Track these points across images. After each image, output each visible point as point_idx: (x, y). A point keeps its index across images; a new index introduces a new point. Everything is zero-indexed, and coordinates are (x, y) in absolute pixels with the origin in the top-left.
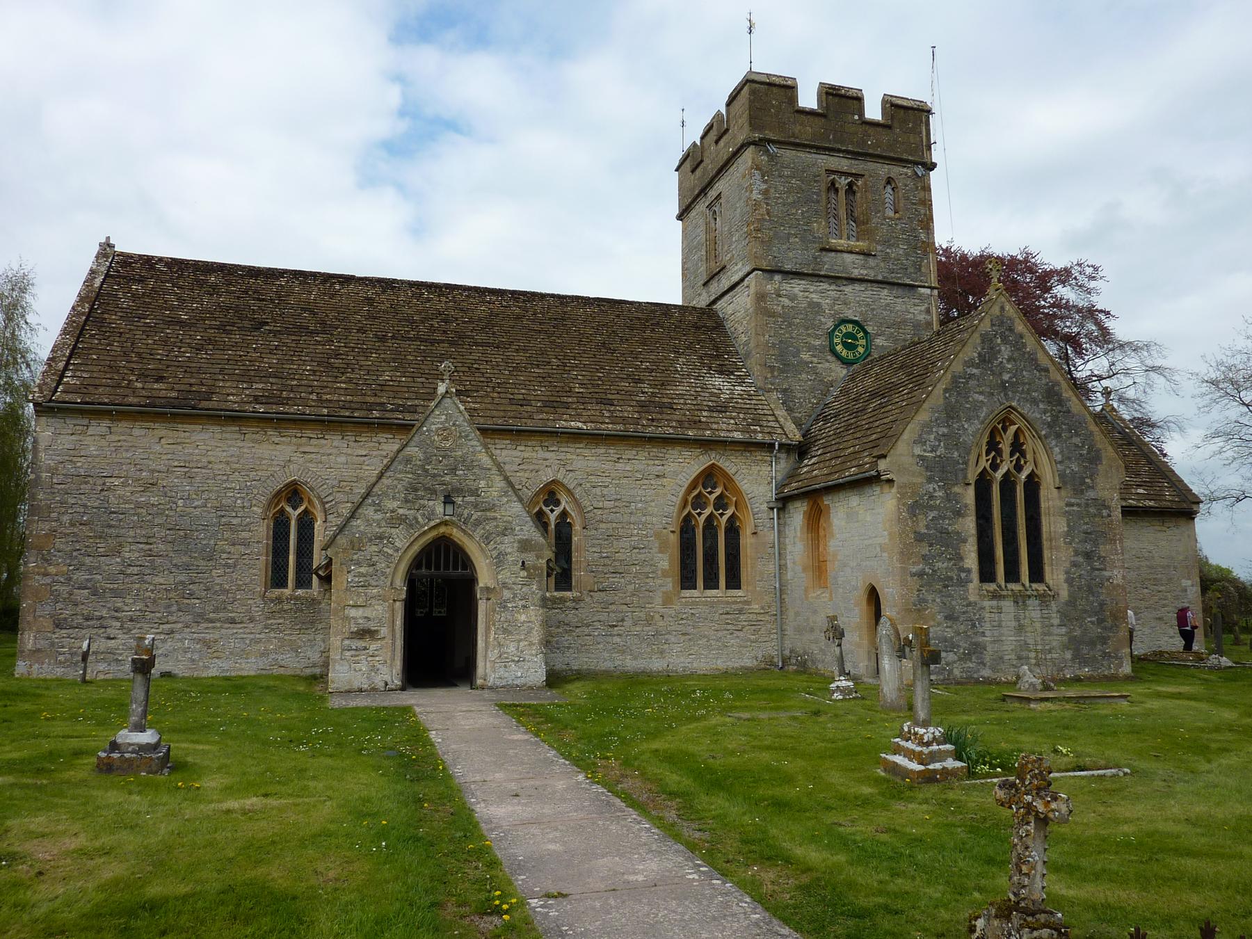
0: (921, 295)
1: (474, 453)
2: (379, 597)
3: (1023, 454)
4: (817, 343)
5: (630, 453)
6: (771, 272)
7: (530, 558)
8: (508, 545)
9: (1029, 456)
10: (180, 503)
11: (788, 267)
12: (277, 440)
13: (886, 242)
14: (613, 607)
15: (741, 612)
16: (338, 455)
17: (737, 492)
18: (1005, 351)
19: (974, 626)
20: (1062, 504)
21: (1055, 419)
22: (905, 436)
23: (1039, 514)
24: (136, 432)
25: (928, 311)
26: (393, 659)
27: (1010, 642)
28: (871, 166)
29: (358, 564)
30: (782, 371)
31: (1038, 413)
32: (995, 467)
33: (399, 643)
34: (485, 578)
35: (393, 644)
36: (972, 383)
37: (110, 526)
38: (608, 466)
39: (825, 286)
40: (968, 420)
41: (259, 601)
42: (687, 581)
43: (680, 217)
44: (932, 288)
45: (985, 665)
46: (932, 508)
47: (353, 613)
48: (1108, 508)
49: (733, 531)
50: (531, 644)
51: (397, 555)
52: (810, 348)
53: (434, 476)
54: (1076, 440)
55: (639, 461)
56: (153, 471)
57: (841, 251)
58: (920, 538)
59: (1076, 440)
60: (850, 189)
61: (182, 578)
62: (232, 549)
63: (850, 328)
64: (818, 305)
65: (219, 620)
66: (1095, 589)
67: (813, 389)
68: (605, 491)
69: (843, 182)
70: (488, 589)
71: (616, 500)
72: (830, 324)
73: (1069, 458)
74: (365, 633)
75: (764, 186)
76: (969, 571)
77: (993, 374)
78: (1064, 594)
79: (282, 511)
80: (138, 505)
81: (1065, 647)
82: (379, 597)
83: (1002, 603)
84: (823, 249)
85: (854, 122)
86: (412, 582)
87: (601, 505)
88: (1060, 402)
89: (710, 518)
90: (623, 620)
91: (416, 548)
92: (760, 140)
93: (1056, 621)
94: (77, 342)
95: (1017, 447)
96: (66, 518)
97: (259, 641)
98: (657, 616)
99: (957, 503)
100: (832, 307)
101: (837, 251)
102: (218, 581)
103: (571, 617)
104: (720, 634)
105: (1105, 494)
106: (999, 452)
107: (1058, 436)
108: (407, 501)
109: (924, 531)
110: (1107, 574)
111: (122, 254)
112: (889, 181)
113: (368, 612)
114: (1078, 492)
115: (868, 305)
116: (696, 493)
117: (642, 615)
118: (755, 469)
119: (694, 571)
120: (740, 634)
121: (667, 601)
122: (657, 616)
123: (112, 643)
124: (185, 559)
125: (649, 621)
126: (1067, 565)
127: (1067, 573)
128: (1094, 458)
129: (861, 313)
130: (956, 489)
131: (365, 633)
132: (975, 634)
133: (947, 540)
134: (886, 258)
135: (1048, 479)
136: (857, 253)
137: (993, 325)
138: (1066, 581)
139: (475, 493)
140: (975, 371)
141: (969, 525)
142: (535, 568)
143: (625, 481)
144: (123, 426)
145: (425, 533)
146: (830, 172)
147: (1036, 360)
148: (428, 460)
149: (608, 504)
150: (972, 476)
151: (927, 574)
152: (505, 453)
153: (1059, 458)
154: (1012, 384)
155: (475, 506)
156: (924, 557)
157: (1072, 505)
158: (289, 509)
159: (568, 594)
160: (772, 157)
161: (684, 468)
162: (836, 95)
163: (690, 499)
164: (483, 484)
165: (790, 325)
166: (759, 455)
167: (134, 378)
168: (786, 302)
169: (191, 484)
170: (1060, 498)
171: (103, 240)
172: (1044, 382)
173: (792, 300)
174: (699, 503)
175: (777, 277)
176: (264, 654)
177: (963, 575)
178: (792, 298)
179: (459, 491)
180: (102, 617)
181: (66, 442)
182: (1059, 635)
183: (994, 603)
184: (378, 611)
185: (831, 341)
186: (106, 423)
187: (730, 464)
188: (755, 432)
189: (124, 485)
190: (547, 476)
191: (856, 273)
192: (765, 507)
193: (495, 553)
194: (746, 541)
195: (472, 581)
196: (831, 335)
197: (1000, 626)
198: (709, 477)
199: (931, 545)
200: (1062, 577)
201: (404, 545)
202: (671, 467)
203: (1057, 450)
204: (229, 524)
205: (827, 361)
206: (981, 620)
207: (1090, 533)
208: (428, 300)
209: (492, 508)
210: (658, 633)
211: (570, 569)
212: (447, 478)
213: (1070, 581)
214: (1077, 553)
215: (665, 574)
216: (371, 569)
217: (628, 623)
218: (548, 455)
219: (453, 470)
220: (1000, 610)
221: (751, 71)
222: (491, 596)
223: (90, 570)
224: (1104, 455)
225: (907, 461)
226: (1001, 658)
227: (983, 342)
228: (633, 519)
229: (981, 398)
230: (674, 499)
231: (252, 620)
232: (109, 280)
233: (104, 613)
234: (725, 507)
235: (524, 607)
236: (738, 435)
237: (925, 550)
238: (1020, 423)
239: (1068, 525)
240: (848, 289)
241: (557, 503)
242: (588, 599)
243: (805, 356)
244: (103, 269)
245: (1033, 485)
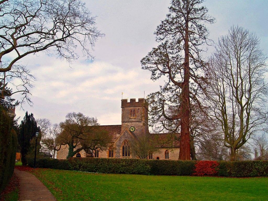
8: (83, 153)
18: (126, 134)
36: (122, 137)
69: (133, 110)
112: (139, 109)
141: (121, 151)
171: (169, 10)
175: (124, 123)
191: (134, 121)
215: (107, 156)
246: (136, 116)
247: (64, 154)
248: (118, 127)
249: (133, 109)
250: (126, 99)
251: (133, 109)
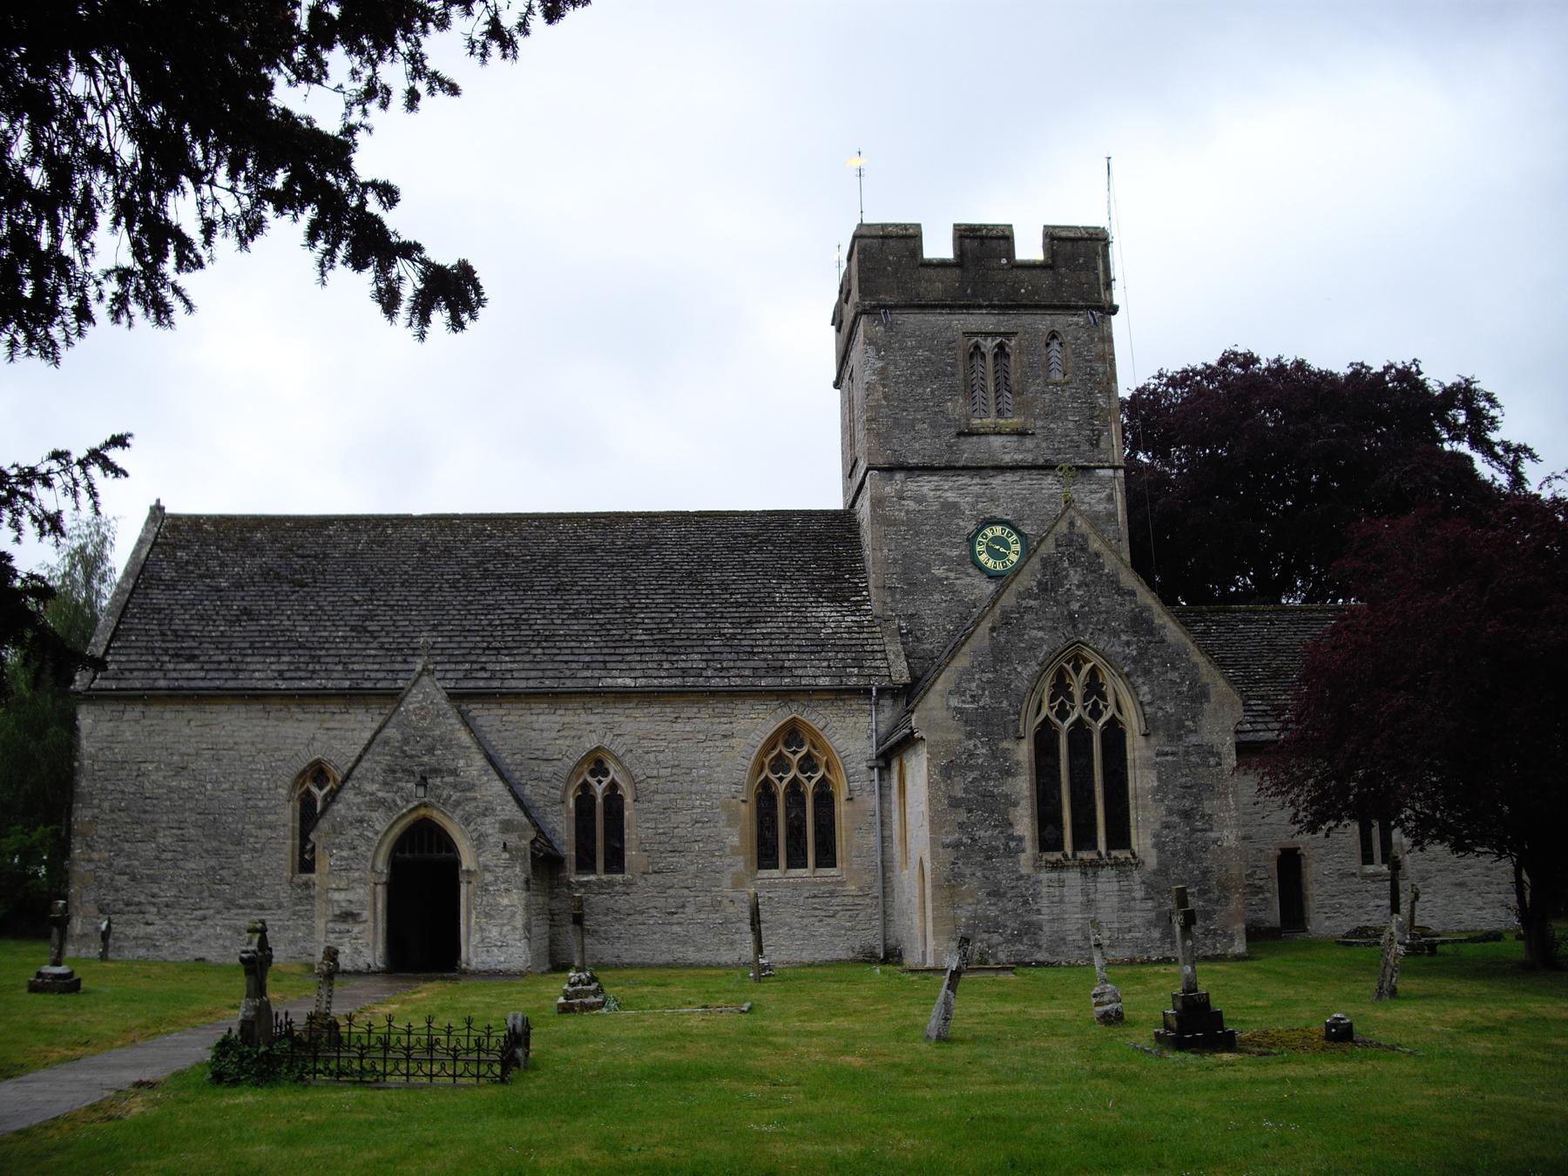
0: (1100, 478)
1: (452, 731)
2: (359, 880)
3: (1103, 697)
4: (955, 553)
5: (690, 711)
6: (890, 469)
7: (512, 840)
8: (490, 826)
9: (1111, 700)
10: (209, 786)
11: (913, 461)
12: (300, 716)
13: (1049, 414)
14: (671, 892)
15: (832, 894)
16: (362, 730)
17: (827, 750)
18: (1075, 577)
19: (1026, 902)
20: (1151, 754)
21: (1142, 652)
22: (939, 686)
23: (1125, 768)
24: (168, 715)
25: (1110, 499)
26: (375, 942)
27: (1074, 919)
28: (1026, 319)
29: (340, 847)
30: (905, 593)
31: (1122, 646)
32: (1062, 714)
33: (381, 926)
34: (467, 861)
35: (375, 927)
37: (145, 812)
38: (663, 727)
39: (964, 480)
40: (1023, 661)
41: (286, 887)
42: (766, 857)
43: (837, 385)
44: (1115, 468)
45: (1040, 947)
46: (972, 768)
47: (336, 896)
48: (1218, 754)
49: (825, 797)
50: (514, 928)
51: (377, 839)
52: (945, 560)
53: (411, 757)
54: (1174, 676)
55: (701, 719)
56: (182, 755)
57: (985, 434)
58: (955, 803)
59: (1174, 676)
60: (1001, 352)
61: (213, 863)
62: (259, 833)
63: (998, 530)
64: (955, 505)
65: (248, 906)
66: (1195, 855)
67: (948, 613)
68: (661, 757)
69: (989, 345)
70: (468, 871)
71: (673, 767)
72: (971, 527)
73: (1162, 698)
74: (348, 916)
75: (880, 364)
76: (1021, 839)
77: (1057, 603)
78: (1152, 861)
79: (308, 792)
80: (171, 790)
81: (1151, 924)
82: (359, 880)
83: (1064, 875)
84: (960, 434)
85: (1002, 268)
86: (395, 863)
87: (655, 773)
88: (1151, 631)
89: (795, 783)
90: (684, 906)
91: (397, 830)
92: (874, 307)
93: (1139, 894)
94: (119, 623)
95: (1094, 687)
96: (106, 805)
97: (287, 928)
98: (726, 901)
99: (1006, 760)
100: (973, 506)
101: (979, 434)
102: (247, 865)
103: (622, 903)
104: (806, 921)
105: (1215, 739)
106: (1070, 697)
107: (1147, 672)
108: (385, 783)
109: (960, 794)
110: (1213, 835)
111: (173, 516)
112: (1054, 336)
113: (351, 896)
114: (1174, 737)
115: (1024, 499)
116: (775, 752)
117: (708, 900)
118: (850, 721)
119: (775, 848)
120: (833, 921)
121: (737, 884)
122: (726, 901)
123: (150, 929)
124: (215, 844)
125: (716, 906)
126: (1157, 826)
127: (1155, 836)
128: (1200, 695)
129: (1015, 510)
130: (1005, 745)
131: (348, 916)
132: (1028, 912)
133: (995, 807)
134: (1050, 435)
135: (1133, 722)
136: (1007, 434)
137: (1058, 546)
138: (1155, 845)
139: (454, 772)
140: (1032, 603)
141: (1023, 786)
142: (517, 849)
143: (685, 744)
144: (155, 709)
145: (404, 815)
146: (969, 334)
147: (1118, 582)
148: (406, 741)
149: (663, 772)
150: (1030, 725)
151: (965, 845)
152: (542, 718)
153: (1148, 698)
154: (1084, 616)
155: (455, 786)
156: (961, 825)
157: (1166, 754)
158: (315, 790)
159: (619, 877)
160: (889, 327)
161: (756, 725)
162: (975, 237)
163: (767, 761)
164: (461, 763)
165: (917, 534)
166: (855, 704)
167: (166, 659)
168: (911, 505)
169: (219, 767)
170: (1148, 747)
172: (1127, 608)
173: (919, 502)
174: (780, 765)
175: (899, 476)
176: (294, 941)
177: (1012, 844)
178: (920, 499)
179: (436, 771)
180: (140, 903)
181: (105, 728)
182: (1143, 911)
183: (1054, 875)
184: (361, 893)
185: (973, 550)
186: (140, 708)
187: (817, 718)
188: (850, 675)
189: (157, 769)
190: (590, 742)
191: (1007, 459)
192: (863, 766)
193: (475, 835)
194: (842, 808)
195: (456, 863)
196: (971, 540)
197: (1061, 901)
198: (792, 733)
199: (970, 811)
200: (1149, 841)
201: (383, 828)
202: (741, 724)
203: (1145, 689)
204: (256, 807)
205: (968, 575)
206: (1035, 896)
207: (1191, 787)
208: (491, 537)
209: (472, 787)
210: (726, 921)
211: (622, 849)
212: (426, 759)
213: (1159, 846)
214: (1170, 812)
216: (352, 853)
217: (690, 910)
218: (592, 718)
219: (431, 750)
220: (1062, 884)
221: (861, 225)
222: (472, 879)
223: (128, 857)
224: (1212, 690)
225: (941, 714)
226: (1063, 939)
227: (1044, 567)
228: (694, 788)
229: (1040, 634)
230: (745, 762)
231: (280, 906)
232: (157, 549)
233: (142, 898)
234: (815, 769)
235: (507, 890)
236: (824, 682)
237: (962, 816)
238: (1095, 660)
239: (1159, 779)
240: (997, 481)
241: (606, 773)
242: (641, 883)
243: (938, 572)
244: (151, 537)
245: (1115, 736)
246: (1024, 408)
247: (164, 839)
248: (478, 534)
249: (988, 334)
250: (905, 227)
251: (988, 334)
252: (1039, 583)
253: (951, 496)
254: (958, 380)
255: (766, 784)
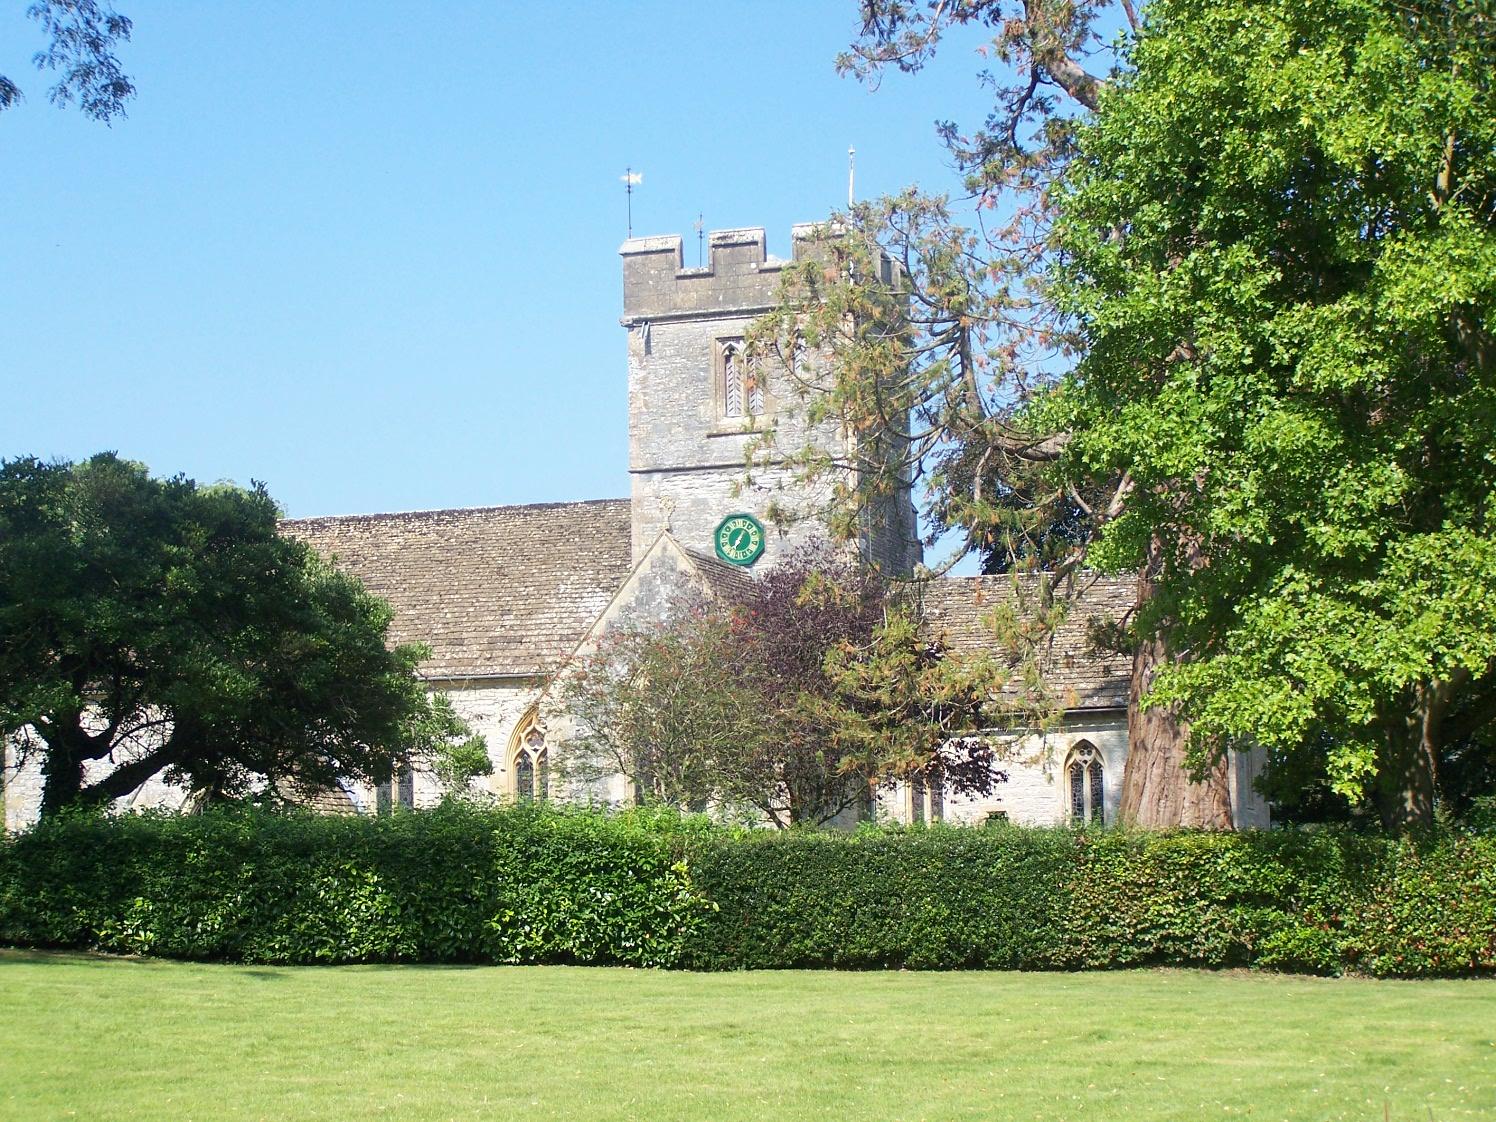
64: (704, 502)
75: (643, 373)
84: (709, 436)
116: (529, 729)
163: (523, 735)
227: (641, 585)
252: (637, 598)
253: (701, 494)
254: (710, 385)
255: (523, 754)
